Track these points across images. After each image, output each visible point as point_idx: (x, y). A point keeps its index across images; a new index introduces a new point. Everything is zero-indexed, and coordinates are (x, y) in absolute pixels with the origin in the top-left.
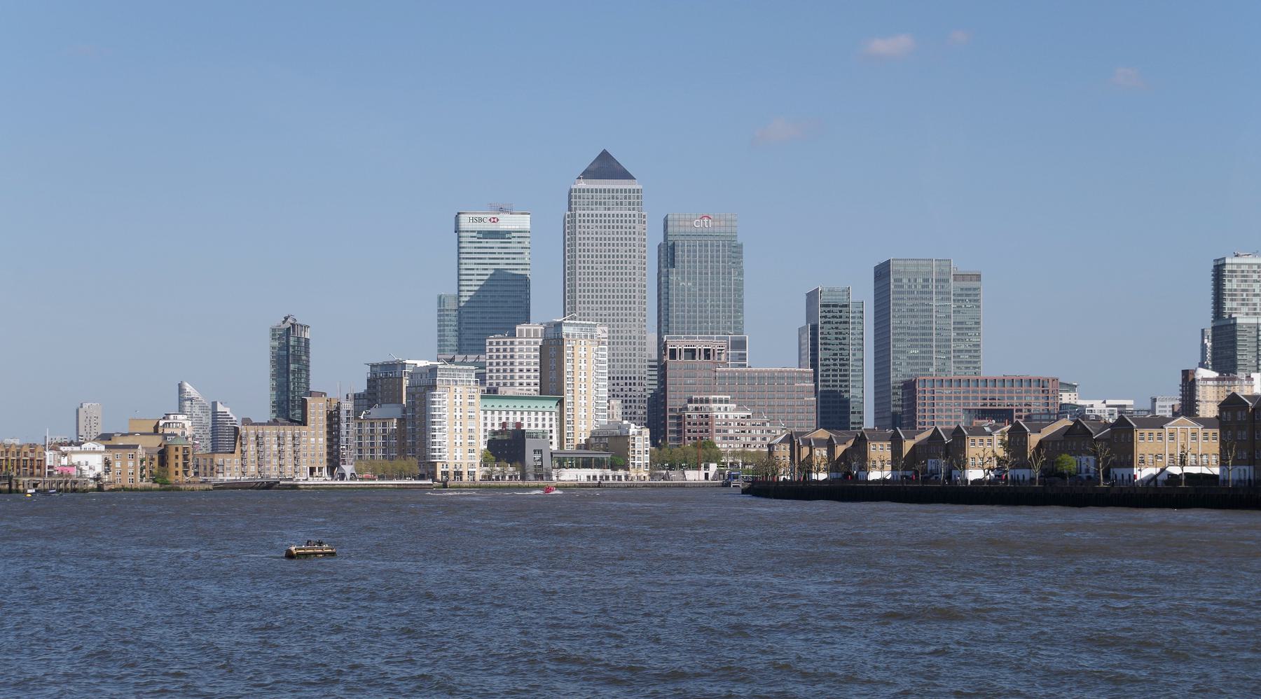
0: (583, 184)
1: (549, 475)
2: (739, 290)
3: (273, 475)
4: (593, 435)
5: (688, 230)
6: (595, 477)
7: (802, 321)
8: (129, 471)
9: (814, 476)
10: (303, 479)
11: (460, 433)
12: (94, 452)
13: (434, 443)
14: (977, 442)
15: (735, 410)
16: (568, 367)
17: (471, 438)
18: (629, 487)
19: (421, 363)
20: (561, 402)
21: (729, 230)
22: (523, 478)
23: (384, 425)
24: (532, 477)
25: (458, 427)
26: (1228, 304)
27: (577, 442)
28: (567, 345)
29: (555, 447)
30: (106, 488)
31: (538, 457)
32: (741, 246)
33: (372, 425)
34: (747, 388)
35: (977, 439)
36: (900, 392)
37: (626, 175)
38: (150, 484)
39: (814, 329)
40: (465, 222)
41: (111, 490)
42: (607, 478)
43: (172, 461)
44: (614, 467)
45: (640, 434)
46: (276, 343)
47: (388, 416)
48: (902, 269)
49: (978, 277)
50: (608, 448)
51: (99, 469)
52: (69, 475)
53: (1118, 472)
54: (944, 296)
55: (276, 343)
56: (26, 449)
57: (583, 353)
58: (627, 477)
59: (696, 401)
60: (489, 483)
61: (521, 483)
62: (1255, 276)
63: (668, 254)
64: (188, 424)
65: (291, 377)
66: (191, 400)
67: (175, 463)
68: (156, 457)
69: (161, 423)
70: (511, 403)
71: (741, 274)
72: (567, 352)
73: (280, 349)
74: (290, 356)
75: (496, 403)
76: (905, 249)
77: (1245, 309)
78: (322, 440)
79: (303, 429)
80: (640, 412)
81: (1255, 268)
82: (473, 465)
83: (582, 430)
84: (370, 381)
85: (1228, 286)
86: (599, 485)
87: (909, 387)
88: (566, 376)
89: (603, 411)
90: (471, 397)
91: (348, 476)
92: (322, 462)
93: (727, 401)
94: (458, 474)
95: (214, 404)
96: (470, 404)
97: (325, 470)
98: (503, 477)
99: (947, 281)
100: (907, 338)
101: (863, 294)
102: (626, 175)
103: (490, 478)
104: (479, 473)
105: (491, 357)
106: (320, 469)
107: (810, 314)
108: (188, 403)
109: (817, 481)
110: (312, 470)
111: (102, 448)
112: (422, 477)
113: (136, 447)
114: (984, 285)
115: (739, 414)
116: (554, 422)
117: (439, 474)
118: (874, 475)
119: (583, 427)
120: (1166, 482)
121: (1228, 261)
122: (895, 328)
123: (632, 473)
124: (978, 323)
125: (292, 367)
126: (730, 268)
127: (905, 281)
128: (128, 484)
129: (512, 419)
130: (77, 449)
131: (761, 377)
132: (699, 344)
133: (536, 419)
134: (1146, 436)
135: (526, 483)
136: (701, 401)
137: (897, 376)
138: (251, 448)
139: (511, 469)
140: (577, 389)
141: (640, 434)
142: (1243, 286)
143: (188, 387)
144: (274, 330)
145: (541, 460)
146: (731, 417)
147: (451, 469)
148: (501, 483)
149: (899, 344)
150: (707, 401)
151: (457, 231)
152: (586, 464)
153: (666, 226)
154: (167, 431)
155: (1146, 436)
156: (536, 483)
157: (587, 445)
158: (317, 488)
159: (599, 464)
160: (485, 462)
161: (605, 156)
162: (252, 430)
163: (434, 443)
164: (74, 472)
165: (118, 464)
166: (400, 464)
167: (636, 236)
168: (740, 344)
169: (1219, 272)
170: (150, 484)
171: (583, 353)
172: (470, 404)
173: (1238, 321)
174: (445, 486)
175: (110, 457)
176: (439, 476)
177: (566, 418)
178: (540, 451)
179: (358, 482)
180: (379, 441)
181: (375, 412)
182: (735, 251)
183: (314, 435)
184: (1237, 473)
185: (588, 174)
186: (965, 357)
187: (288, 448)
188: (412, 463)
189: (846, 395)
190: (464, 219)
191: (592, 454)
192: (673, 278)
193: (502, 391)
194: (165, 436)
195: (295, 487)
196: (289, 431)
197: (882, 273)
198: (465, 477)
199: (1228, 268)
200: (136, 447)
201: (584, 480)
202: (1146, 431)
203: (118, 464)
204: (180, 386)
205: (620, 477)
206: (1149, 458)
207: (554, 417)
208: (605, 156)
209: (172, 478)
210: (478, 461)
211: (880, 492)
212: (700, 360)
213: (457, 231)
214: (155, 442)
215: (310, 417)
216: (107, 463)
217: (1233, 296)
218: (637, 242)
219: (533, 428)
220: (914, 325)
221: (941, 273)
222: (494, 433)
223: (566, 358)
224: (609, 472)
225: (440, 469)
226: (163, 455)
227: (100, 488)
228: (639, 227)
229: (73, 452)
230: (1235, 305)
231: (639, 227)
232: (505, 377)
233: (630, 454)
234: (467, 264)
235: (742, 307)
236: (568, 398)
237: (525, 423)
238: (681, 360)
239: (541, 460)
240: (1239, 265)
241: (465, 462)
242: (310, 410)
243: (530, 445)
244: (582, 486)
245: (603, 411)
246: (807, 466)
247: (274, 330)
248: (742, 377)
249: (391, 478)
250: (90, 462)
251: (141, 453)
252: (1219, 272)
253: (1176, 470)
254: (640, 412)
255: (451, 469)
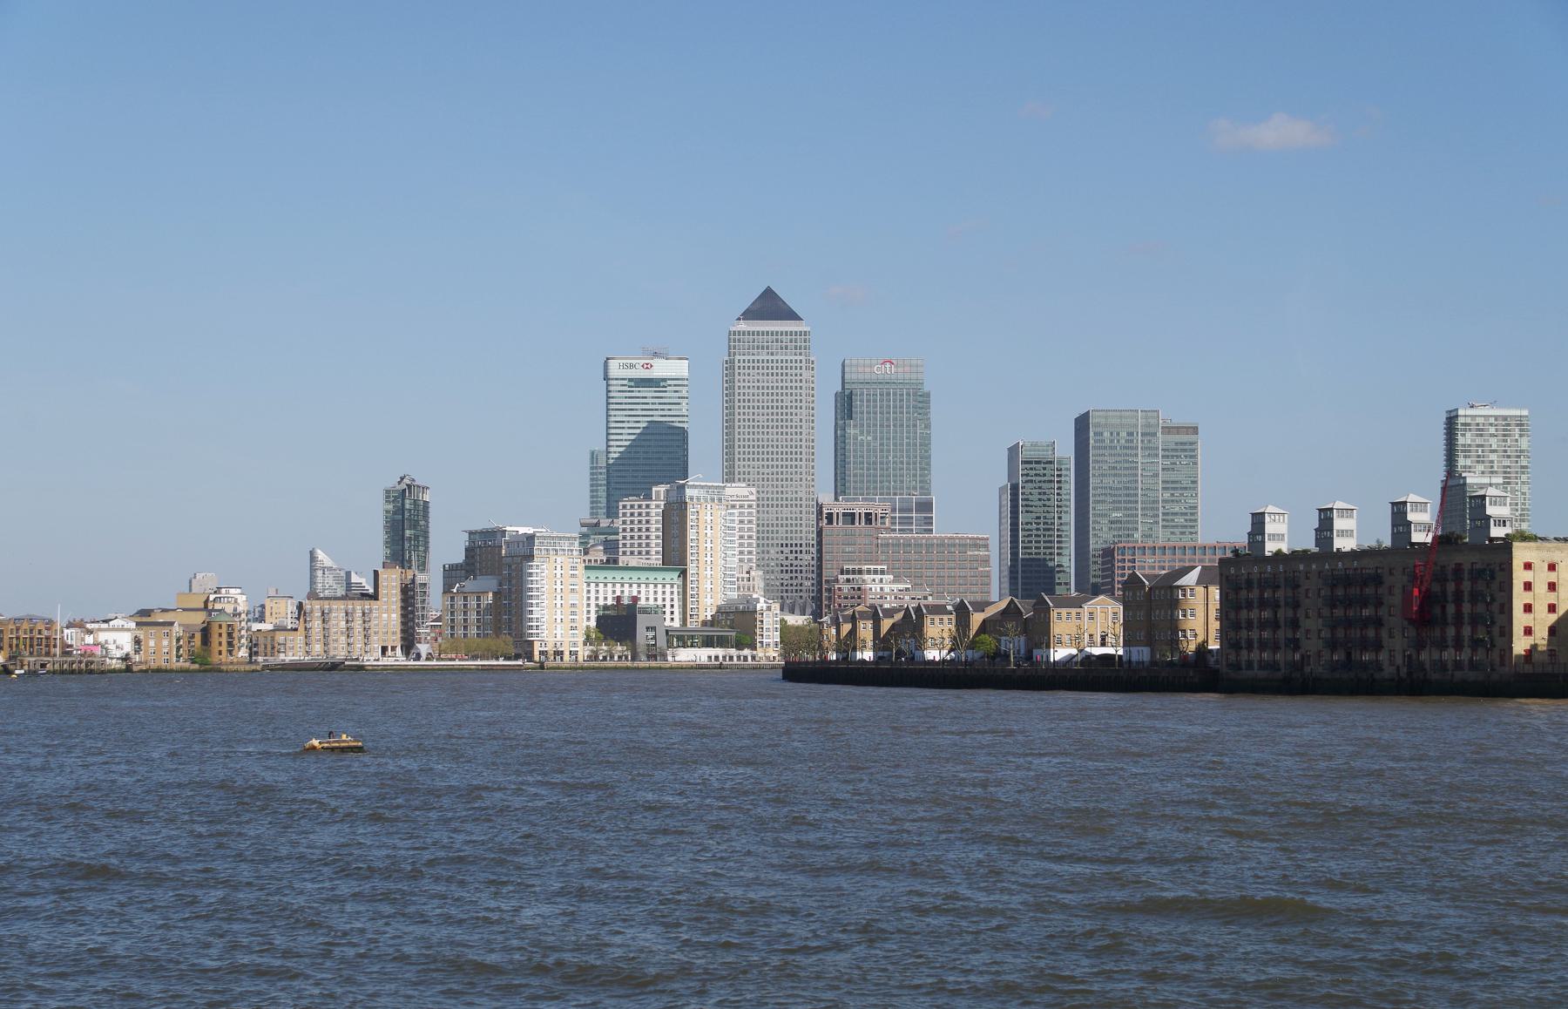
0: (743, 326)
1: (664, 656)
2: (926, 443)
3: (339, 653)
4: (720, 610)
5: (867, 376)
6: (717, 658)
7: (1004, 481)
8: (162, 650)
9: (859, 656)
10: (372, 659)
11: (562, 609)
12: (122, 629)
13: (531, 620)
14: (937, 621)
15: (894, 582)
16: (691, 534)
17: (573, 613)
18: (754, 668)
19: (522, 530)
20: (684, 573)
21: (914, 376)
22: (633, 659)
23: (479, 599)
24: (643, 658)
25: (559, 602)
26: (1461, 462)
27: (702, 618)
28: (690, 510)
29: (677, 624)
30: (135, 668)
31: (650, 634)
32: (928, 395)
33: (465, 599)
34: (913, 556)
35: (937, 618)
36: (1100, 560)
37: (792, 316)
38: (187, 665)
39: (1015, 488)
40: (615, 369)
41: (141, 671)
42: (731, 658)
43: (215, 639)
44: (739, 646)
45: (769, 609)
46: (390, 507)
47: (484, 591)
48: (1103, 421)
49: (1195, 430)
50: (736, 625)
51: (128, 648)
52: (92, 655)
53: (1036, 652)
54: (1151, 451)
55: (390, 507)
56: (40, 626)
57: (709, 518)
58: (753, 658)
59: (848, 572)
60: (592, 664)
61: (629, 664)
62: (1492, 430)
63: (846, 404)
64: (242, 599)
65: (407, 545)
66: (323, 569)
67: (219, 641)
68: (198, 636)
69: (212, 597)
70: (635, 575)
71: (928, 426)
72: (690, 517)
73: (395, 513)
74: (406, 525)
75: (618, 575)
76: (1106, 397)
77: (1480, 467)
78: (396, 617)
79: (375, 605)
80: (807, 583)
81: (1492, 420)
82: (575, 644)
83: (708, 603)
84: (469, 551)
85: (1461, 440)
86: (721, 667)
87: (1108, 553)
88: (689, 544)
89: (732, 583)
90: (574, 568)
91: (424, 656)
92: (396, 639)
93: (882, 572)
94: (559, 653)
95: (348, 574)
96: (573, 576)
97: (399, 650)
98: (612, 657)
99: (1155, 434)
100: (1109, 499)
101: (1066, 450)
102: (792, 316)
103: (596, 658)
104: (583, 652)
105: (624, 522)
106: (393, 648)
107: (1012, 472)
108: (319, 573)
109: (933, 662)
110: (384, 649)
111: (133, 625)
112: (517, 657)
113: (172, 624)
114: (1201, 440)
115: (895, 587)
116: (675, 596)
117: (536, 653)
118: (932, 654)
119: (709, 601)
120: (1082, 663)
121: (1461, 412)
122: (1095, 488)
123: (760, 653)
124: (1195, 482)
125: (408, 533)
126: (915, 419)
127: (1107, 434)
128: (164, 665)
129: (628, 592)
130: (105, 626)
131: (942, 544)
132: (860, 508)
133: (654, 592)
134: (1064, 615)
135: (636, 664)
136: (854, 572)
137: (1095, 544)
138: (316, 624)
139: (619, 648)
140: (702, 558)
141: (769, 609)
142: (1479, 441)
143: (320, 555)
144: (387, 491)
145: (655, 638)
146: (887, 590)
147: (550, 648)
148: (609, 664)
149: (1099, 507)
150: (860, 572)
151: (606, 378)
152: (708, 642)
153: (843, 373)
154: (218, 606)
155: (1064, 615)
156: (647, 664)
157: (713, 622)
158: (385, 668)
159: (722, 642)
160: (588, 640)
161: (769, 294)
162: (317, 605)
163: (531, 620)
164: (98, 651)
165: (152, 643)
166: (492, 643)
167: (804, 384)
168: (926, 506)
169: (1451, 422)
170: (187, 665)
171: (709, 518)
172: (573, 576)
173: (1469, 481)
174: (542, 667)
175: (141, 634)
176: (537, 658)
177: (689, 592)
178: (654, 629)
179: (434, 663)
180: (473, 617)
181: (469, 585)
182: (921, 401)
183: (387, 611)
184: (1142, 654)
185: (748, 315)
186: (1180, 520)
187: (357, 625)
188: (506, 642)
189: (1050, 564)
190: (613, 364)
191: (716, 632)
192: (851, 431)
193: (622, 561)
194: (210, 612)
195: (361, 668)
196: (358, 607)
197: (1082, 424)
198: (566, 657)
199: (1461, 420)
200: (172, 624)
201: (704, 660)
202: (1064, 611)
203: (152, 643)
204: (312, 553)
205: (746, 658)
206: (1066, 639)
207: (675, 589)
208: (769, 294)
209: (215, 659)
210: (582, 639)
211: (1091, 675)
212: (860, 525)
213: (606, 378)
214: (198, 619)
215: (382, 591)
216: (137, 641)
217: (1467, 451)
218: (804, 392)
219: (651, 602)
220: (1116, 485)
221: (1149, 425)
222: (606, 607)
223: (689, 523)
224: (733, 652)
225: (537, 648)
226: (206, 632)
227: (128, 669)
228: (806, 374)
229: (100, 630)
230: (1468, 462)
231: (806, 374)
232: (640, 545)
233: (758, 631)
234: (617, 416)
235: (929, 464)
236: (691, 569)
237: (643, 596)
238: (839, 525)
239: (655, 638)
240: (1473, 417)
241: (567, 640)
242: (382, 583)
243: (642, 621)
244: (700, 667)
245: (732, 583)
246: (848, 644)
247: (387, 491)
248: (929, 546)
249: (475, 658)
250: (118, 641)
251: (177, 630)
252: (1451, 422)
253: (1098, 651)
254: (807, 583)
255: (550, 648)
